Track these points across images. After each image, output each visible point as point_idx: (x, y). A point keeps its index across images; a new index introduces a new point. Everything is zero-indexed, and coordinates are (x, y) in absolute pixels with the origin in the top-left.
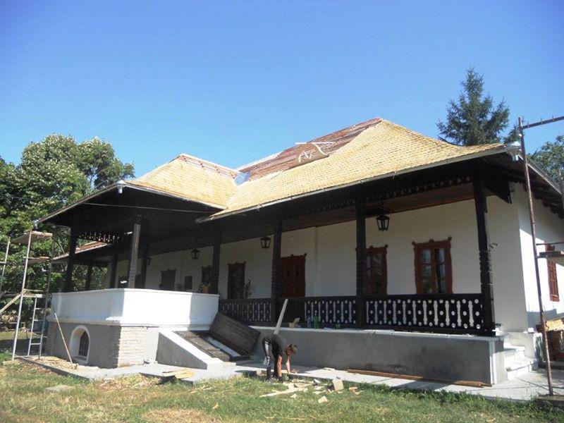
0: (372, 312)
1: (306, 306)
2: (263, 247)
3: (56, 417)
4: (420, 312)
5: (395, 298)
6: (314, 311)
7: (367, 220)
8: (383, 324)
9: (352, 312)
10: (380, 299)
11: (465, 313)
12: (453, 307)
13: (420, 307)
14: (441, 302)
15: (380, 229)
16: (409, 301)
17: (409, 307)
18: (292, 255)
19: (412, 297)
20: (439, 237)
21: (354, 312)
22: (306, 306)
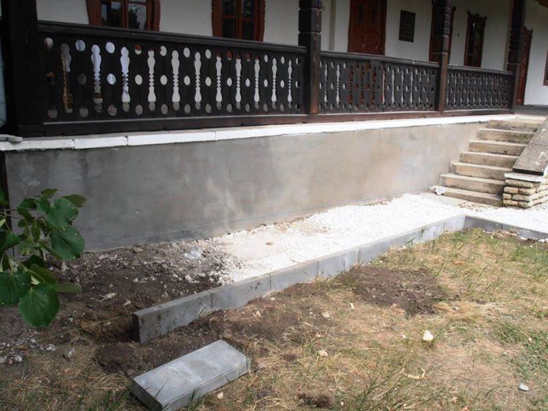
5: (176, 43)
11: (164, 80)
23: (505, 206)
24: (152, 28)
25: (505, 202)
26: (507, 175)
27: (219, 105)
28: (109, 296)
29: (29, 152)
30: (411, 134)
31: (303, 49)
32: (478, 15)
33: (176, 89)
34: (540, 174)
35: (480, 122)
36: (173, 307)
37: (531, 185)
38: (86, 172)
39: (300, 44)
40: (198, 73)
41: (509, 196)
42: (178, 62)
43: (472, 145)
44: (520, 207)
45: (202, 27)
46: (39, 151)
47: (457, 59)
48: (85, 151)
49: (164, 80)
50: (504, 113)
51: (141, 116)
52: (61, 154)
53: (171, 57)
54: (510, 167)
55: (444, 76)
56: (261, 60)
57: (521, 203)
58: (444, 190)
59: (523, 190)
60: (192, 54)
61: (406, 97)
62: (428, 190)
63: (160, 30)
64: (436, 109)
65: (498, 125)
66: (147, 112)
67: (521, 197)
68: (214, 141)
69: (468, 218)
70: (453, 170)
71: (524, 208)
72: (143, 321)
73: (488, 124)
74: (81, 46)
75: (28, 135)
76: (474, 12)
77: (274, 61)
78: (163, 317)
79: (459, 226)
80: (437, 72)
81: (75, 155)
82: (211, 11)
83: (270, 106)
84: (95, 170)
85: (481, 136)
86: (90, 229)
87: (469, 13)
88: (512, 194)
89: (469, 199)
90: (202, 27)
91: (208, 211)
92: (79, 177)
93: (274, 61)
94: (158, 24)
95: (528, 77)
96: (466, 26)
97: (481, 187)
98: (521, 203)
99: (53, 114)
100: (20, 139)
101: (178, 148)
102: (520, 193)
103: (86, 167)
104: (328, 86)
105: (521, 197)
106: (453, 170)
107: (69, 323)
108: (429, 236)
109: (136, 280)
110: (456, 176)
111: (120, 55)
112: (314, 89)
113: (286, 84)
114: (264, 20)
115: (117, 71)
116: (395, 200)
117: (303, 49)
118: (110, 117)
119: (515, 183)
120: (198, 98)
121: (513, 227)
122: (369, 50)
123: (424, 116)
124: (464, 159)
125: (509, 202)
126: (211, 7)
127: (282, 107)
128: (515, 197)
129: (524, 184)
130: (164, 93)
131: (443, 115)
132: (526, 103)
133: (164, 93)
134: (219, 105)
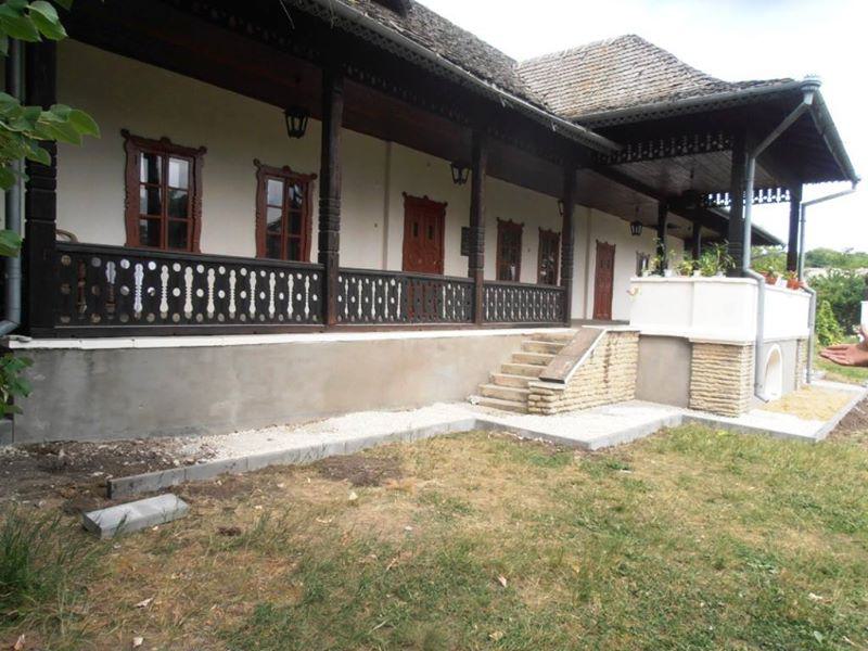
0: (177, 292)
1: (444, 293)
2: (455, 181)
3: (519, 642)
4: (222, 294)
5: (213, 262)
6: (389, 299)
7: (320, 123)
8: (249, 320)
9: (311, 298)
10: (177, 261)
11: (222, 294)
12: (200, 281)
13: (263, 285)
14: (152, 266)
15: (455, 181)
16: (222, 270)
17: (243, 283)
18: (426, 197)
19: (251, 265)
20: (611, 243)
21: (315, 298)
22: (444, 293)
23: (531, 413)
24: (192, 251)
25: (530, 409)
26: (530, 384)
27: (307, 316)
28: (96, 474)
29: (37, 350)
30: (440, 345)
31: (472, 280)
32: (511, 221)
33: (272, 302)
34: (562, 382)
35: (523, 335)
36: (145, 478)
37: (552, 392)
38: (92, 370)
39: (469, 275)
40: (291, 290)
41: (533, 403)
42: (214, 278)
43: (514, 356)
44: (543, 414)
45: (247, 248)
46: (47, 349)
47: (489, 273)
48: (92, 351)
49: (243, 295)
50: (558, 326)
51: (152, 323)
52: (68, 354)
53: (161, 272)
54: (537, 376)
55: (480, 290)
56: (363, 282)
57: (544, 410)
58: (479, 399)
59: (544, 397)
60: (304, 277)
61: (458, 310)
62: (465, 400)
63: (445, 274)
64: (474, 321)
65: (542, 338)
66: (206, 319)
67: (543, 405)
68: (221, 346)
69: (478, 421)
70: (492, 380)
71: (546, 414)
72: (116, 487)
73: (532, 337)
74: (244, 272)
75: (36, 336)
76: (506, 218)
77: (360, 282)
78: (135, 485)
79: (469, 427)
80: (475, 284)
81: (81, 354)
82: (255, 228)
83: (356, 317)
84: (100, 369)
85: (525, 348)
86: (91, 421)
87: (498, 219)
88: (536, 402)
89: (500, 407)
90: (247, 248)
91: (215, 409)
92: (84, 374)
93: (360, 282)
94: (198, 244)
95: (614, 292)
96: (538, 244)
97: (514, 397)
98: (544, 410)
99: (65, 320)
100: (29, 339)
101: (184, 351)
102: (543, 400)
103: (92, 364)
104: (350, 298)
105: (543, 405)
106: (492, 380)
107: (50, 488)
108: (427, 435)
109: (126, 463)
110: (496, 387)
111: (229, 276)
112: (331, 301)
113: (383, 300)
114: (200, 221)
115: (302, 291)
116: (425, 409)
117: (472, 280)
118: (197, 323)
119: (538, 390)
120: (290, 310)
121: (514, 428)
122: (427, 269)
123: (459, 328)
124: (505, 370)
125: (533, 409)
126: (254, 224)
127: (353, 318)
128: (539, 404)
129: (546, 392)
130: (243, 305)
131: (481, 327)
132: (614, 318)
133: (243, 305)
134: (307, 316)
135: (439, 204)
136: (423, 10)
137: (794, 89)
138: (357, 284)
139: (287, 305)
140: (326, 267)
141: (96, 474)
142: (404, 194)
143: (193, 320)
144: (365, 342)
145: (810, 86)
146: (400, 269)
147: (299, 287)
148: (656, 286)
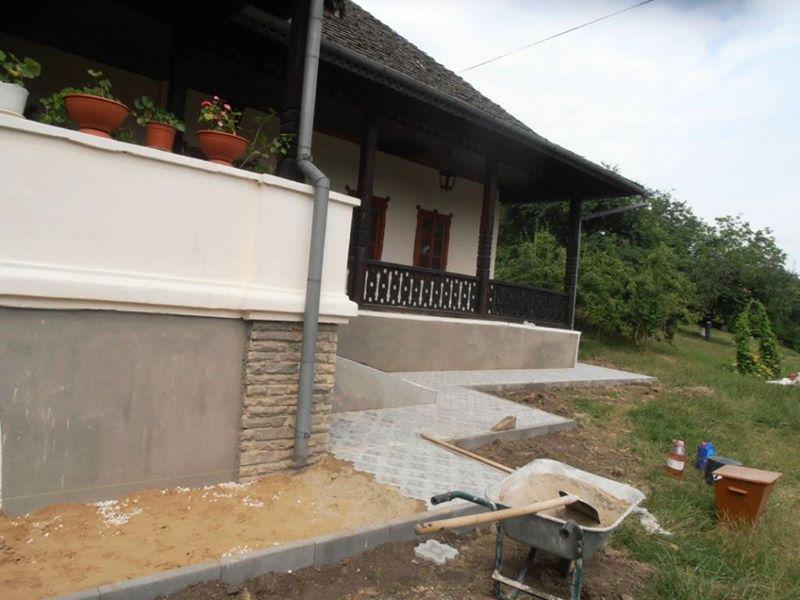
15: (442, 187)
18: (435, 211)
28: (68, 424)
39: (477, 275)
56: (404, 275)
66: (407, 304)
135: (445, 216)
136: (357, 9)
137: (792, 275)
138: (450, 283)
139: (375, 291)
140: (356, 258)
141: (68, 424)
142: (418, 207)
143: (390, 303)
144: (412, 321)
145: (796, 275)
146: (475, 275)
147: (465, 289)
148: (159, 170)
